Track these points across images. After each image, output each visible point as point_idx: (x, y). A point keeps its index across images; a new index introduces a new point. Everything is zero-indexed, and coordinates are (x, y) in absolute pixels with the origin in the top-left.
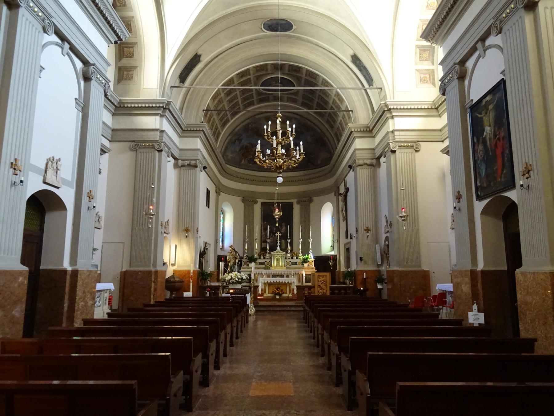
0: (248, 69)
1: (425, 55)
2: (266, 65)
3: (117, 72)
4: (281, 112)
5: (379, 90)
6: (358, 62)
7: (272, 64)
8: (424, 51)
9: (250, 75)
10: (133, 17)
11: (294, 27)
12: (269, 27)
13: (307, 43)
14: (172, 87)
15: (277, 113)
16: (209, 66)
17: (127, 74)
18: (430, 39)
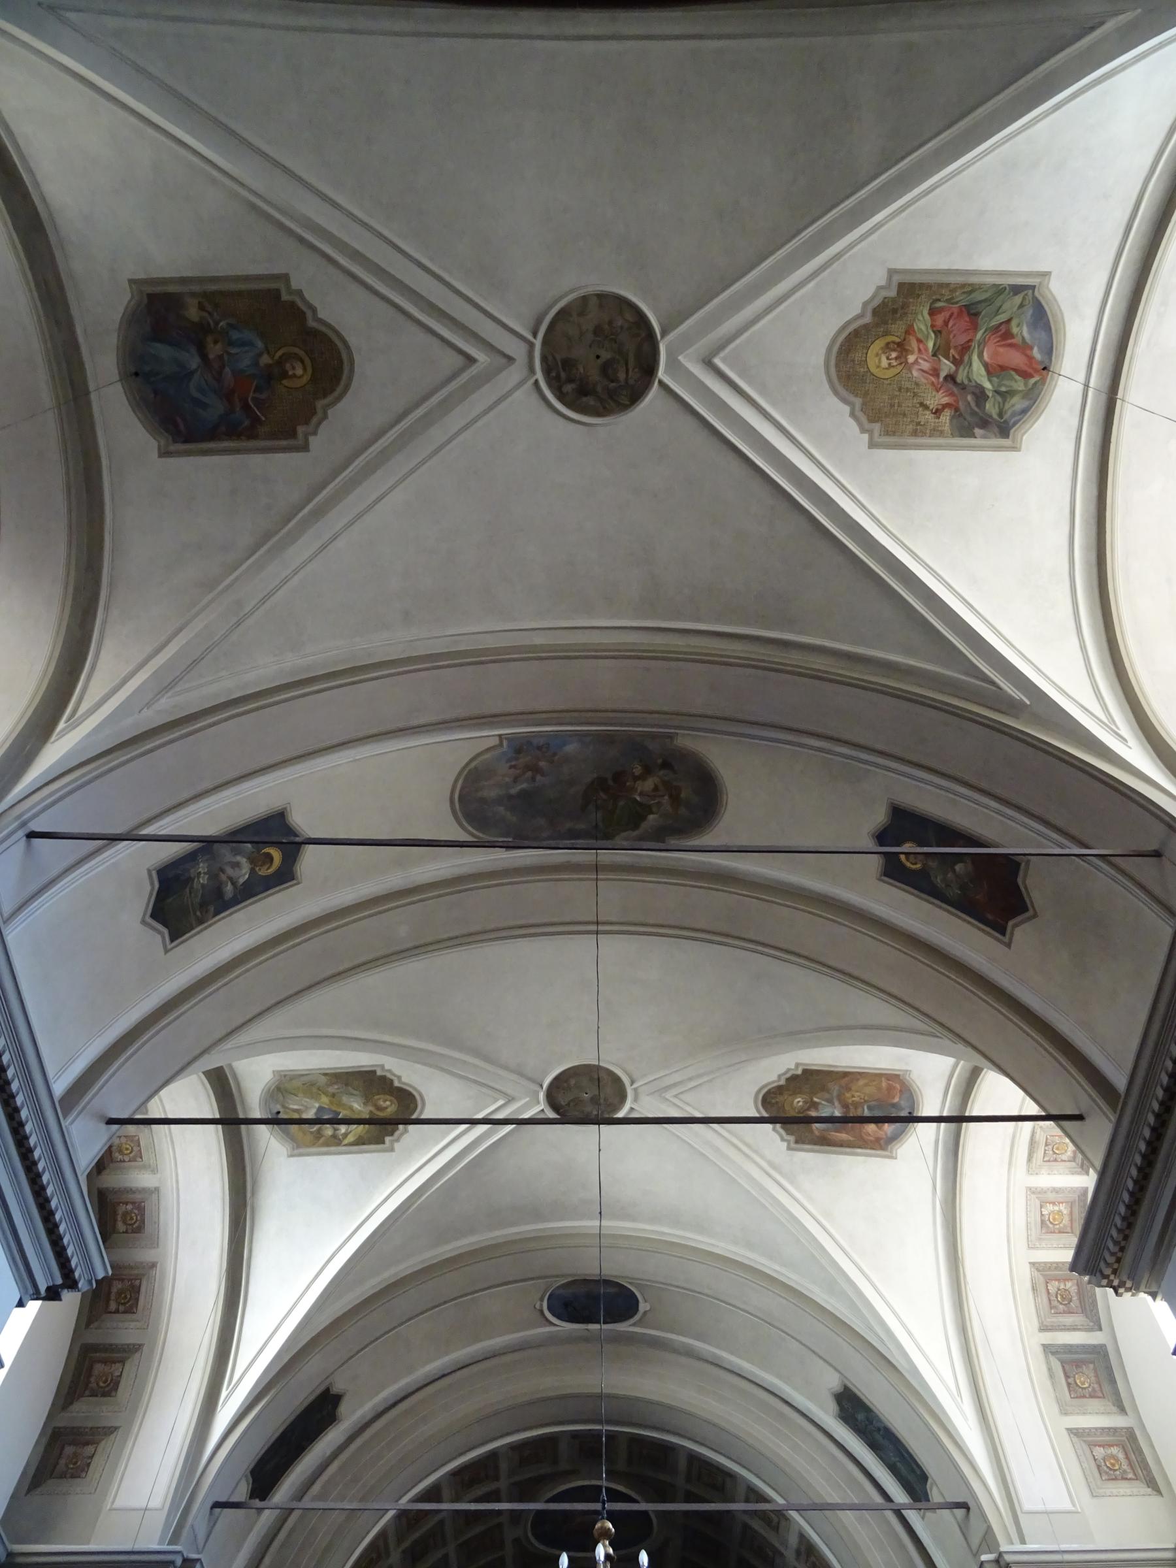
0: (493, 1455)
1: (1085, 1379)
2: (552, 1439)
3: (41, 1449)
4: (611, 1516)
5: (960, 1513)
6: (861, 1416)
7: (575, 1435)
8: (1078, 1364)
9: (497, 1478)
10: (153, 1265)
11: (643, 1307)
12: (566, 1305)
13: (684, 1360)
14: (217, 1505)
15: (596, 1515)
16: (359, 1442)
17: (75, 1455)
18: (1108, 1271)
